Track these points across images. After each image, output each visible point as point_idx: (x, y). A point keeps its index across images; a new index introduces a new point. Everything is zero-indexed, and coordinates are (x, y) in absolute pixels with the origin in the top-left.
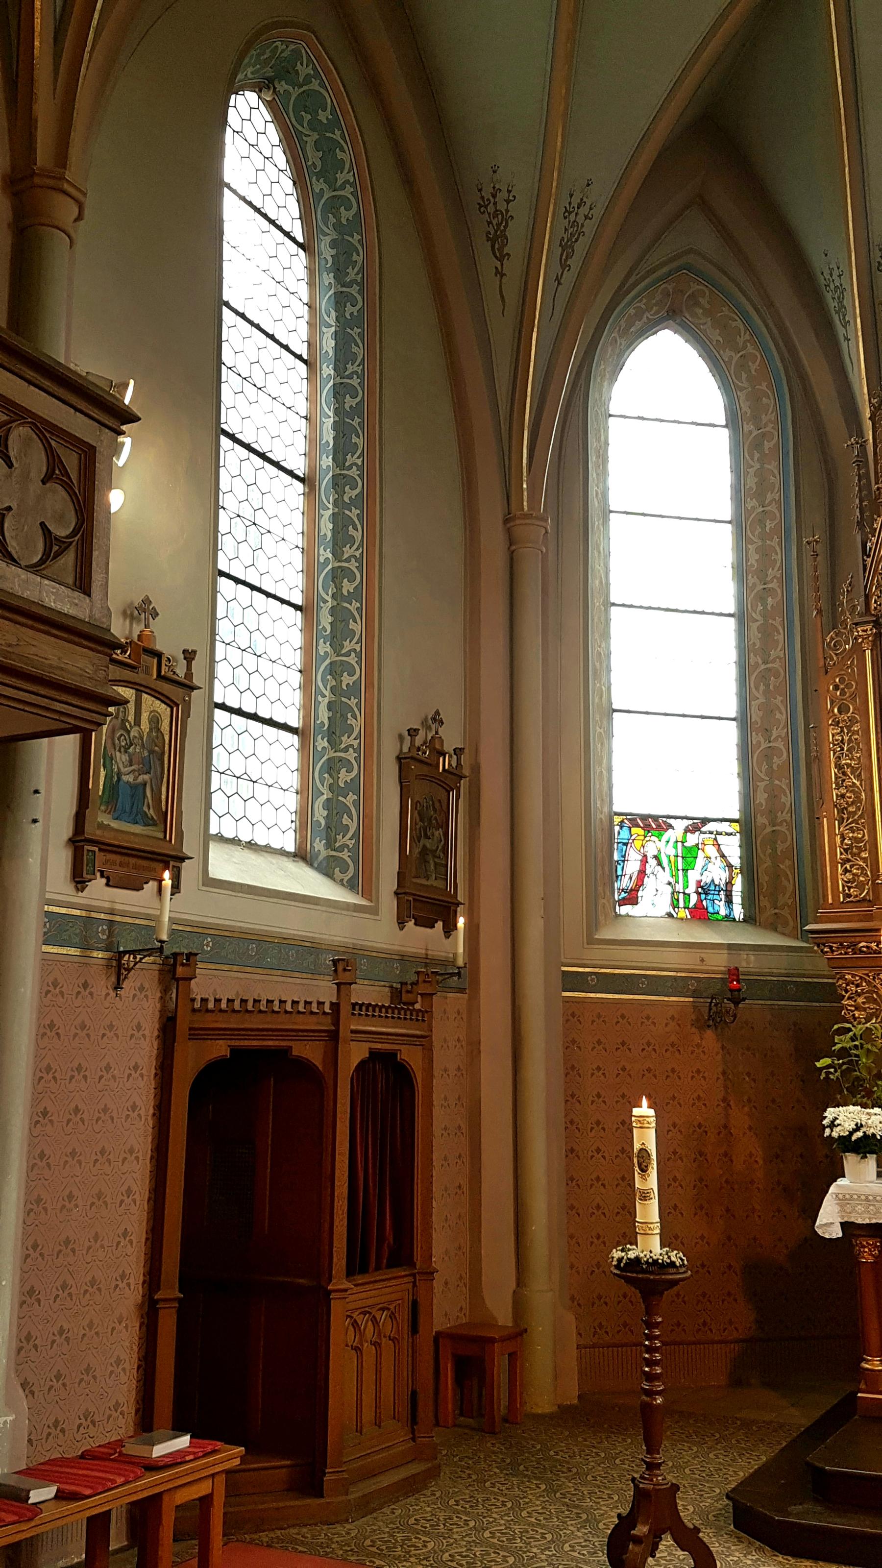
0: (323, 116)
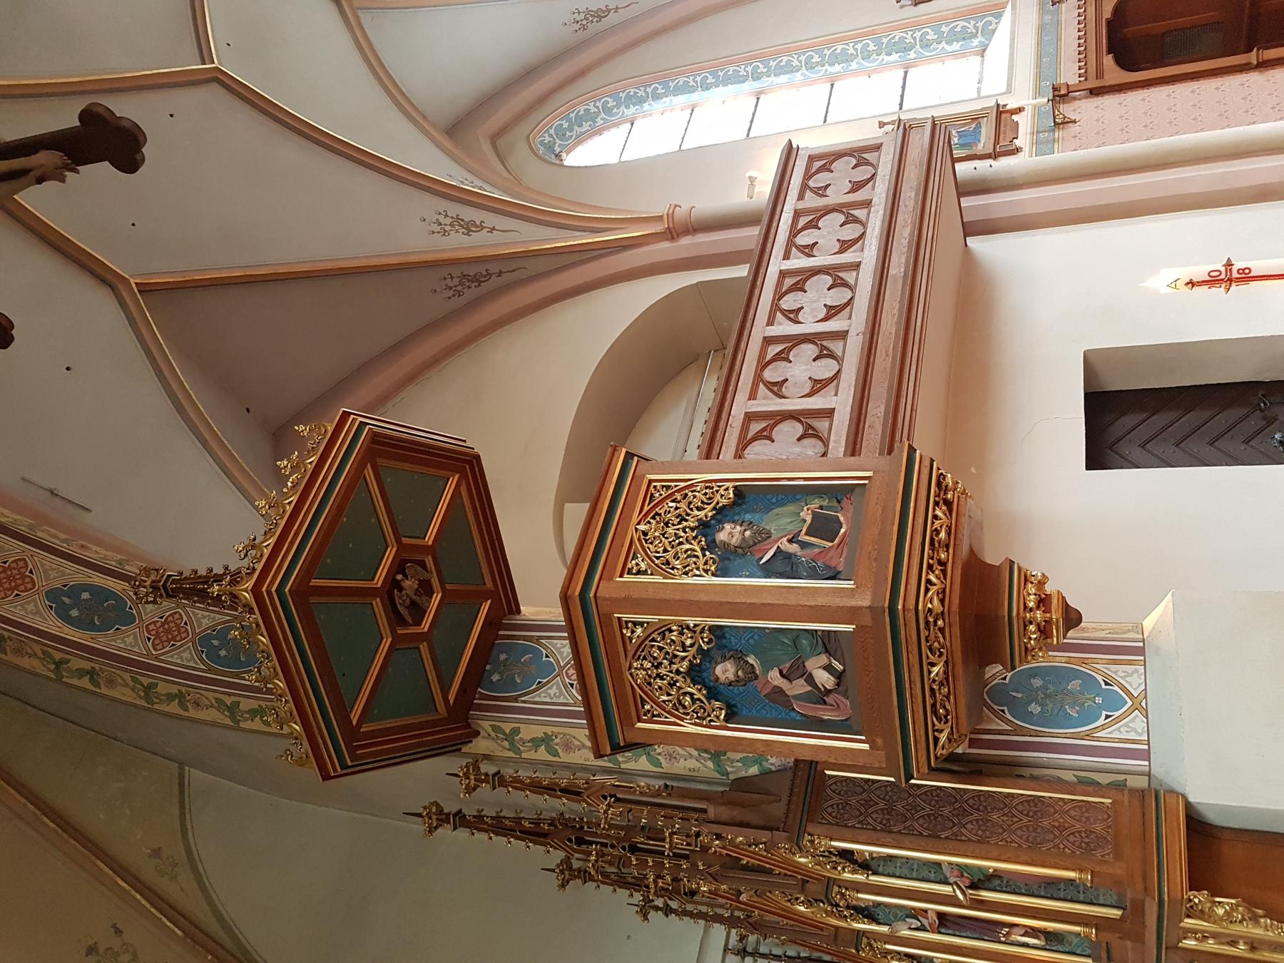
0: (566, 125)
